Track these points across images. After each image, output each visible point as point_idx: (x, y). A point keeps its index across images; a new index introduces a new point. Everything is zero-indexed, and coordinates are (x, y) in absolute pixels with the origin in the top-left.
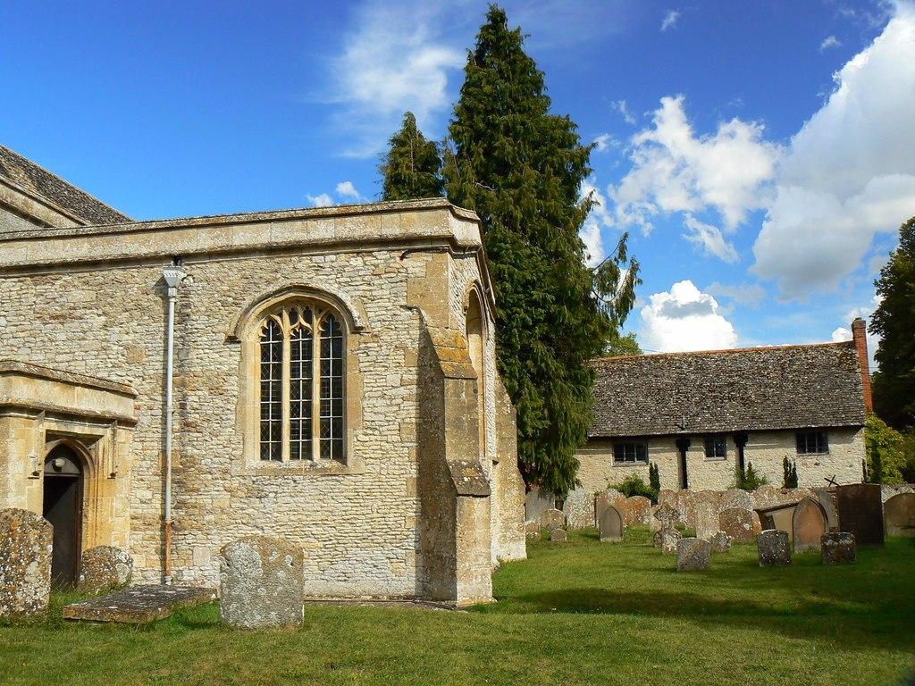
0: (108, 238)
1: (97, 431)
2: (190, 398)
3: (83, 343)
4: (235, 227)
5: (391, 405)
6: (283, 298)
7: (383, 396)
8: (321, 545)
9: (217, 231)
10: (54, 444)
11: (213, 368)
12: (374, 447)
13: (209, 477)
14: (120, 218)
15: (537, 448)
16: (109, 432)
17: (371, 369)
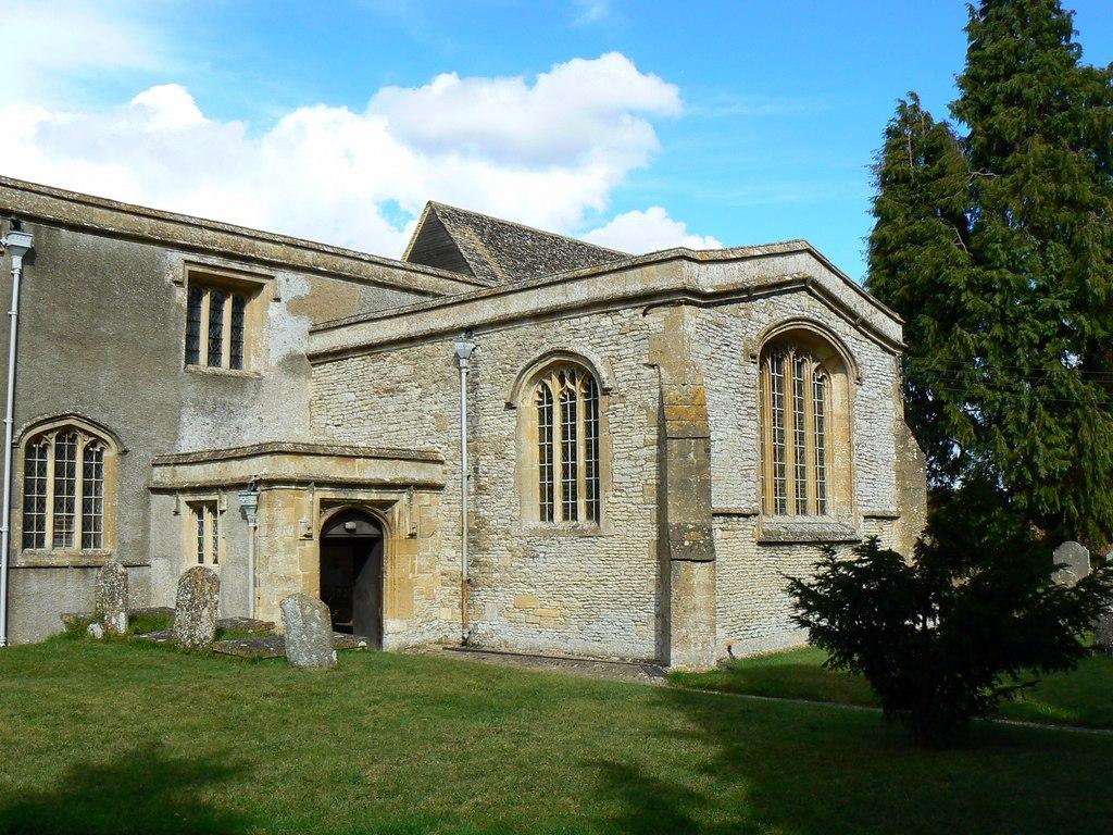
0: (420, 314)
1: (391, 496)
2: (482, 463)
3: (405, 413)
4: (511, 296)
5: (636, 466)
6: (548, 363)
7: (628, 458)
8: (580, 604)
9: (498, 301)
10: (330, 512)
11: (496, 433)
12: (622, 509)
13: (496, 537)
14: (621, 257)
15: (1062, 494)
16: (405, 497)
17: (619, 430)
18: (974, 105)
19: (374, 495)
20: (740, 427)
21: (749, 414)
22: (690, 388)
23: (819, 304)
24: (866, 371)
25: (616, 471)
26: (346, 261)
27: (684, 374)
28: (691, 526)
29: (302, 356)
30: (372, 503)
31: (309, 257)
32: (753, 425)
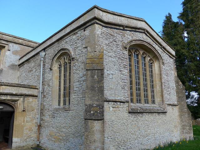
1: (17, 98)
6: (60, 54)
16: (22, 99)
18: (183, 16)
19: (9, 98)
20: (120, 71)
21: (124, 67)
22: (97, 53)
23: (149, 39)
24: (165, 62)
25: (75, 87)
26: (32, 43)
27: (95, 48)
28: (95, 105)
29: (16, 65)
30: (8, 100)
31: (20, 41)
32: (126, 71)
